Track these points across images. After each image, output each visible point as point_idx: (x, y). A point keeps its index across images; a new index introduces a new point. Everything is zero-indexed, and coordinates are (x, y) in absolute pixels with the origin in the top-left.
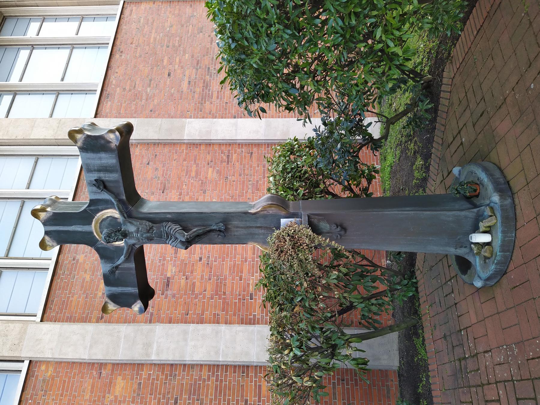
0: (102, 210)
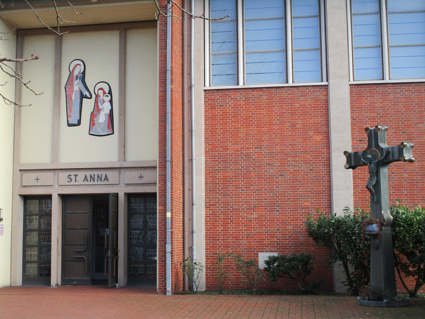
0: (380, 152)
